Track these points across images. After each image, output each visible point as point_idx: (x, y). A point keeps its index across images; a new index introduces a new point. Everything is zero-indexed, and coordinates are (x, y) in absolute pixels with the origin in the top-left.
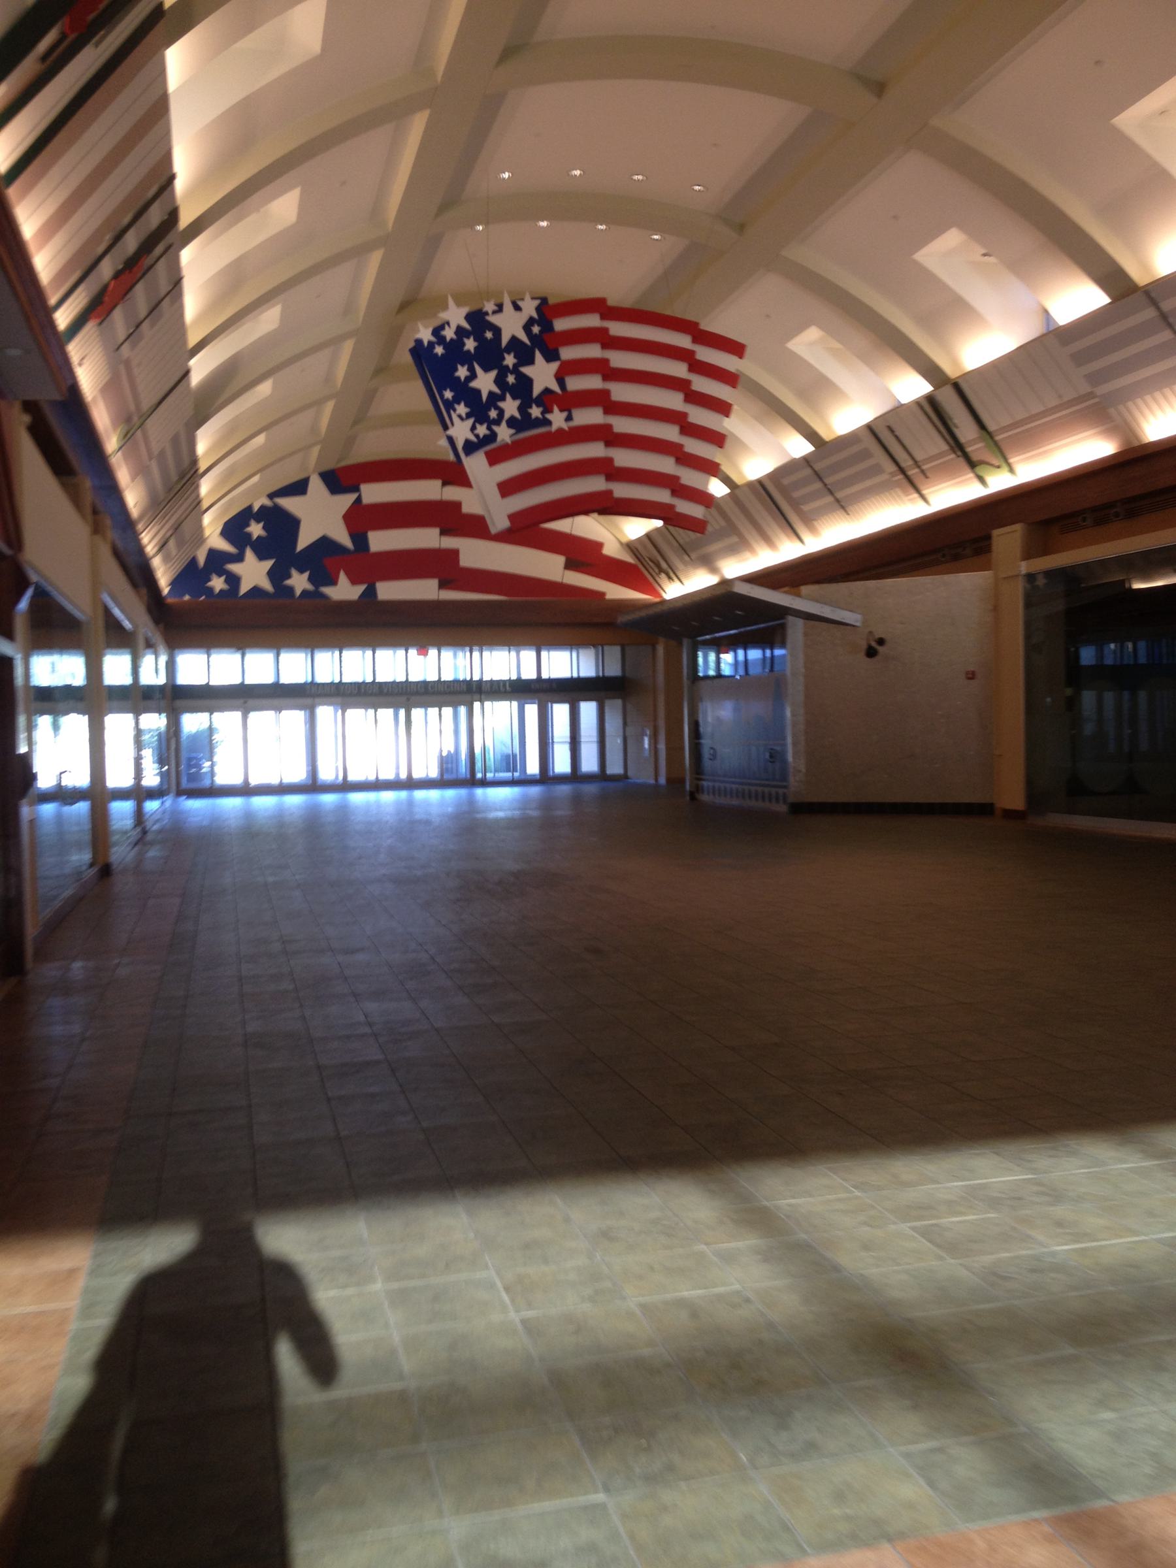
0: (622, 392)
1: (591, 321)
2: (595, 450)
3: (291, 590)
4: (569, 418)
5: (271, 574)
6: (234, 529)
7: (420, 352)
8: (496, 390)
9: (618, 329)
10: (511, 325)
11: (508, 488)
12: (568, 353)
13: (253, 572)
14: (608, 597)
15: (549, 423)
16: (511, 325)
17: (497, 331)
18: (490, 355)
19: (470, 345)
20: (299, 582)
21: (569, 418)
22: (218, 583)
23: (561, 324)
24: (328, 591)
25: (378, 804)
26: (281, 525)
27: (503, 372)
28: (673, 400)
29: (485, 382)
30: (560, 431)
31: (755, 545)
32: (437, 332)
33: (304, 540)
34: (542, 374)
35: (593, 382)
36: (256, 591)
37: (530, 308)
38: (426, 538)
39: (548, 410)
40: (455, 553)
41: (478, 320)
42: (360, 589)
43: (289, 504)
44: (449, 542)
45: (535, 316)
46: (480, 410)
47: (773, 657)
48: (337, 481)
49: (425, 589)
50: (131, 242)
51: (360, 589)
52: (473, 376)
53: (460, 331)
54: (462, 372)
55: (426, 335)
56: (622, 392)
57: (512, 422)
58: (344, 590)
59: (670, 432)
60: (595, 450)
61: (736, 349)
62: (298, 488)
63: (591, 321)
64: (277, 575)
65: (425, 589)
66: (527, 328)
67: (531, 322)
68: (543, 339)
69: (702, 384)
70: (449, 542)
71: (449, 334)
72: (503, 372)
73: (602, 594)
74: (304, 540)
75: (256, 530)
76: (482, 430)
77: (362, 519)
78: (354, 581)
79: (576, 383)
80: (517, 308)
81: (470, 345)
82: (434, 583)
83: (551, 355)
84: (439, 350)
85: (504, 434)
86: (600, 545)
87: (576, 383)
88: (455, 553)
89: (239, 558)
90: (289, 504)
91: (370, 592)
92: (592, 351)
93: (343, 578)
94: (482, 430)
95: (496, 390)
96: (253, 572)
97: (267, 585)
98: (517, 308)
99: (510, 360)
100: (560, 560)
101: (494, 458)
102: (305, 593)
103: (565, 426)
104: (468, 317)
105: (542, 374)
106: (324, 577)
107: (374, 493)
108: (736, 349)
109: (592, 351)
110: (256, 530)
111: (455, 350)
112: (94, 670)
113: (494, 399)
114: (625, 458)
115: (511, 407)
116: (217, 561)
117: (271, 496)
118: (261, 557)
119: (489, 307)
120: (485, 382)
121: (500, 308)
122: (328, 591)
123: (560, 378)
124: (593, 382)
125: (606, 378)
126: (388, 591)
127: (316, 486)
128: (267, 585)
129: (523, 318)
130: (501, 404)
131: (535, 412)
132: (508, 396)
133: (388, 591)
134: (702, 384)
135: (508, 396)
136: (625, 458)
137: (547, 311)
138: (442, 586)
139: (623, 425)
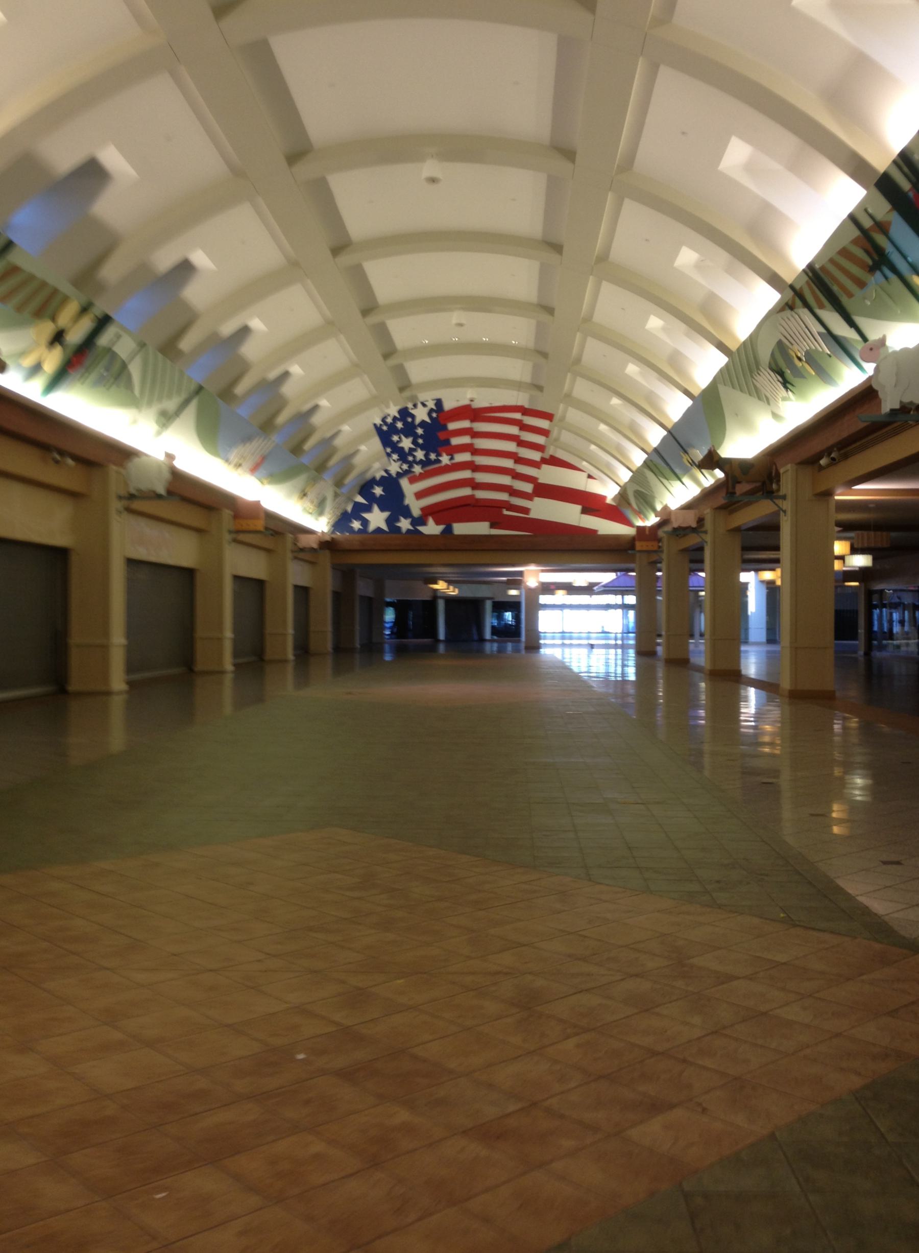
2: (466, 474)
3: (399, 528)
4: (452, 458)
7: (378, 429)
8: (412, 446)
11: (419, 495)
13: (377, 518)
14: (599, 533)
15: (439, 461)
17: (413, 417)
18: (409, 430)
19: (399, 425)
21: (452, 458)
24: (421, 528)
25: (236, 642)
28: (511, 447)
29: (406, 443)
30: (447, 465)
31: (644, 510)
32: (384, 420)
35: (465, 440)
36: (379, 530)
41: (404, 413)
42: (441, 528)
45: (434, 407)
46: (403, 456)
49: (481, 528)
51: (441, 528)
53: (395, 419)
54: (395, 438)
55: (378, 421)
57: (421, 462)
58: (432, 528)
60: (466, 474)
61: (549, 416)
64: (390, 521)
65: (481, 528)
67: (431, 411)
71: (389, 420)
73: (594, 532)
75: (378, 491)
76: (405, 467)
81: (399, 425)
82: (486, 525)
84: (385, 428)
85: (417, 469)
89: (368, 509)
91: (448, 530)
94: (405, 467)
95: (412, 446)
96: (377, 518)
97: (384, 527)
100: (578, 508)
101: (413, 480)
102: (408, 531)
103: (448, 463)
104: (400, 412)
108: (549, 416)
111: (393, 429)
114: (482, 477)
115: (420, 455)
118: (382, 509)
119: (410, 406)
120: (406, 443)
121: (415, 406)
122: (421, 528)
124: (465, 440)
126: (460, 529)
128: (384, 527)
130: (415, 454)
133: (460, 529)
136: (482, 477)
138: (492, 526)
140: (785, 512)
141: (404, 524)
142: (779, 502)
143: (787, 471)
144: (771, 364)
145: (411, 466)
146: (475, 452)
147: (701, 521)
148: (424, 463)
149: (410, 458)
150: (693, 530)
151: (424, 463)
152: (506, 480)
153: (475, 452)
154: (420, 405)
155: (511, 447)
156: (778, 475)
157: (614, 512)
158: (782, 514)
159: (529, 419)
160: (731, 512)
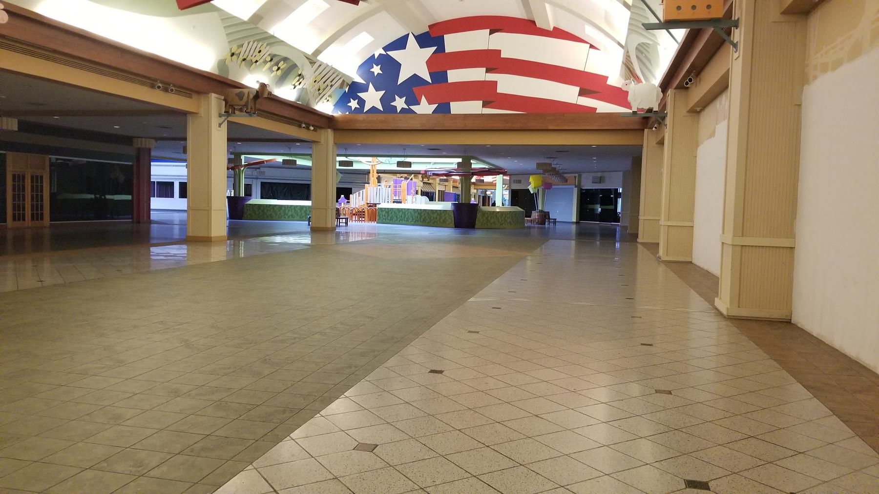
13: (373, 98)
20: (400, 103)
22: (354, 104)
26: (391, 66)
33: (403, 77)
36: (373, 110)
38: (478, 74)
40: (495, 84)
43: (393, 54)
44: (491, 77)
47: (245, 166)
48: (424, 40)
49: (474, 107)
62: (400, 44)
65: (474, 107)
70: (491, 77)
74: (403, 77)
75: (376, 70)
77: (441, 63)
86: (606, 78)
88: (495, 84)
90: (393, 54)
93: (423, 99)
106: (413, 100)
107: (454, 43)
112: (443, 108)
117: (387, 48)
118: (377, 89)
126: (458, 108)
127: (412, 42)
132: (371, 86)
133: (458, 108)
135: (371, 86)
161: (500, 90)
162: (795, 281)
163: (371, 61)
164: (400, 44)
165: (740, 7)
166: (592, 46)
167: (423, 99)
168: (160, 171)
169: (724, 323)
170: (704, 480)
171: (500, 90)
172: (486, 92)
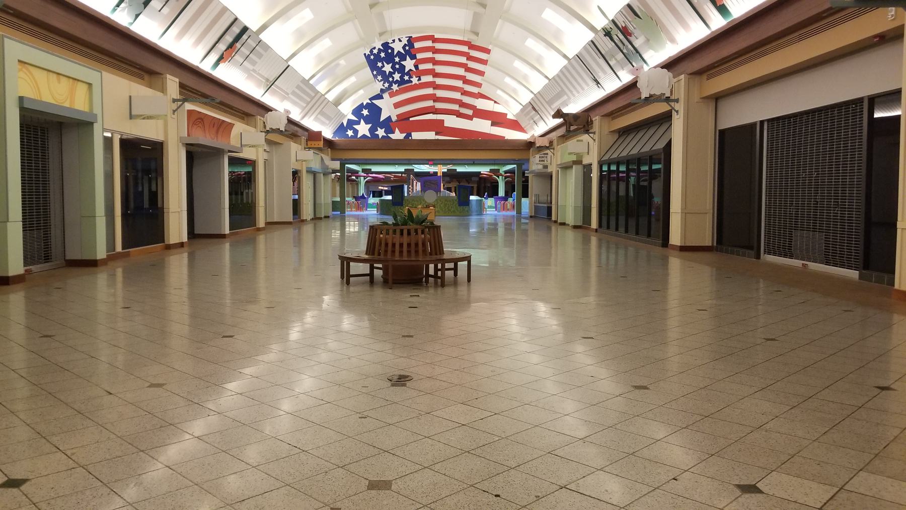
0: (440, 69)
1: (429, 43)
2: (430, 91)
5: (370, 130)
6: (357, 111)
7: (367, 57)
9: (439, 46)
10: (398, 47)
11: (397, 105)
12: (419, 56)
13: (363, 129)
16: (398, 47)
17: (393, 49)
18: (390, 58)
19: (383, 55)
20: (381, 132)
21: (419, 79)
22: (350, 133)
23: (417, 45)
26: (375, 111)
27: (394, 64)
28: (460, 71)
29: (388, 68)
32: (371, 51)
34: (409, 64)
35: (429, 66)
36: (364, 136)
37: (405, 41)
39: (411, 77)
40: (443, 121)
41: (386, 46)
46: (386, 77)
49: (430, 135)
50: (229, 38)
52: (383, 66)
54: (380, 64)
55: (368, 53)
56: (440, 69)
57: (397, 82)
58: (398, 135)
59: (459, 83)
60: (430, 91)
61: (487, 51)
62: (379, 97)
63: (429, 43)
64: (372, 130)
66: (404, 48)
68: (410, 50)
69: (472, 65)
71: (375, 51)
72: (394, 64)
75: (365, 112)
76: (387, 85)
78: (401, 132)
79: (422, 67)
80: (400, 41)
81: (383, 55)
83: (413, 57)
85: (395, 87)
87: (422, 67)
88: (443, 121)
89: (358, 123)
92: (429, 55)
93: (397, 130)
96: (363, 129)
98: (400, 41)
99: (397, 59)
101: (392, 95)
104: (382, 45)
105: (409, 64)
106: (390, 130)
108: (487, 51)
109: (429, 55)
110: (365, 112)
111: (377, 57)
113: (391, 74)
114: (440, 93)
115: (397, 76)
116: (351, 123)
117: (370, 99)
118: (366, 123)
119: (390, 41)
120: (388, 68)
123: (416, 66)
124: (429, 66)
125: (434, 64)
126: (416, 136)
129: (402, 44)
131: (406, 78)
133: (416, 136)
134: (472, 65)
136: (440, 93)
137: (411, 41)
139: (439, 81)
140: (677, 112)
141: (381, 132)
142: (672, 104)
143: (596, 119)
144: (581, 66)
145: (390, 85)
146: (436, 75)
147: (551, 143)
148: (401, 82)
149: (391, 79)
150: (547, 148)
151: (401, 82)
152: (457, 95)
153: (436, 75)
154: (397, 41)
155: (460, 71)
156: (592, 121)
157: (515, 125)
158: (674, 113)
159: (473, 52)
160: (613, 119)
161: (446, 125)
162: (165, 154)
163: (361, 107)
164: (379, 97)
165: (109, 176)
166: (495, 102)
167: (397, 130)
168: (389, 197)
169: (195, 162)
170: (747, 495)
171: (446, 125)
172: (438, 126)
